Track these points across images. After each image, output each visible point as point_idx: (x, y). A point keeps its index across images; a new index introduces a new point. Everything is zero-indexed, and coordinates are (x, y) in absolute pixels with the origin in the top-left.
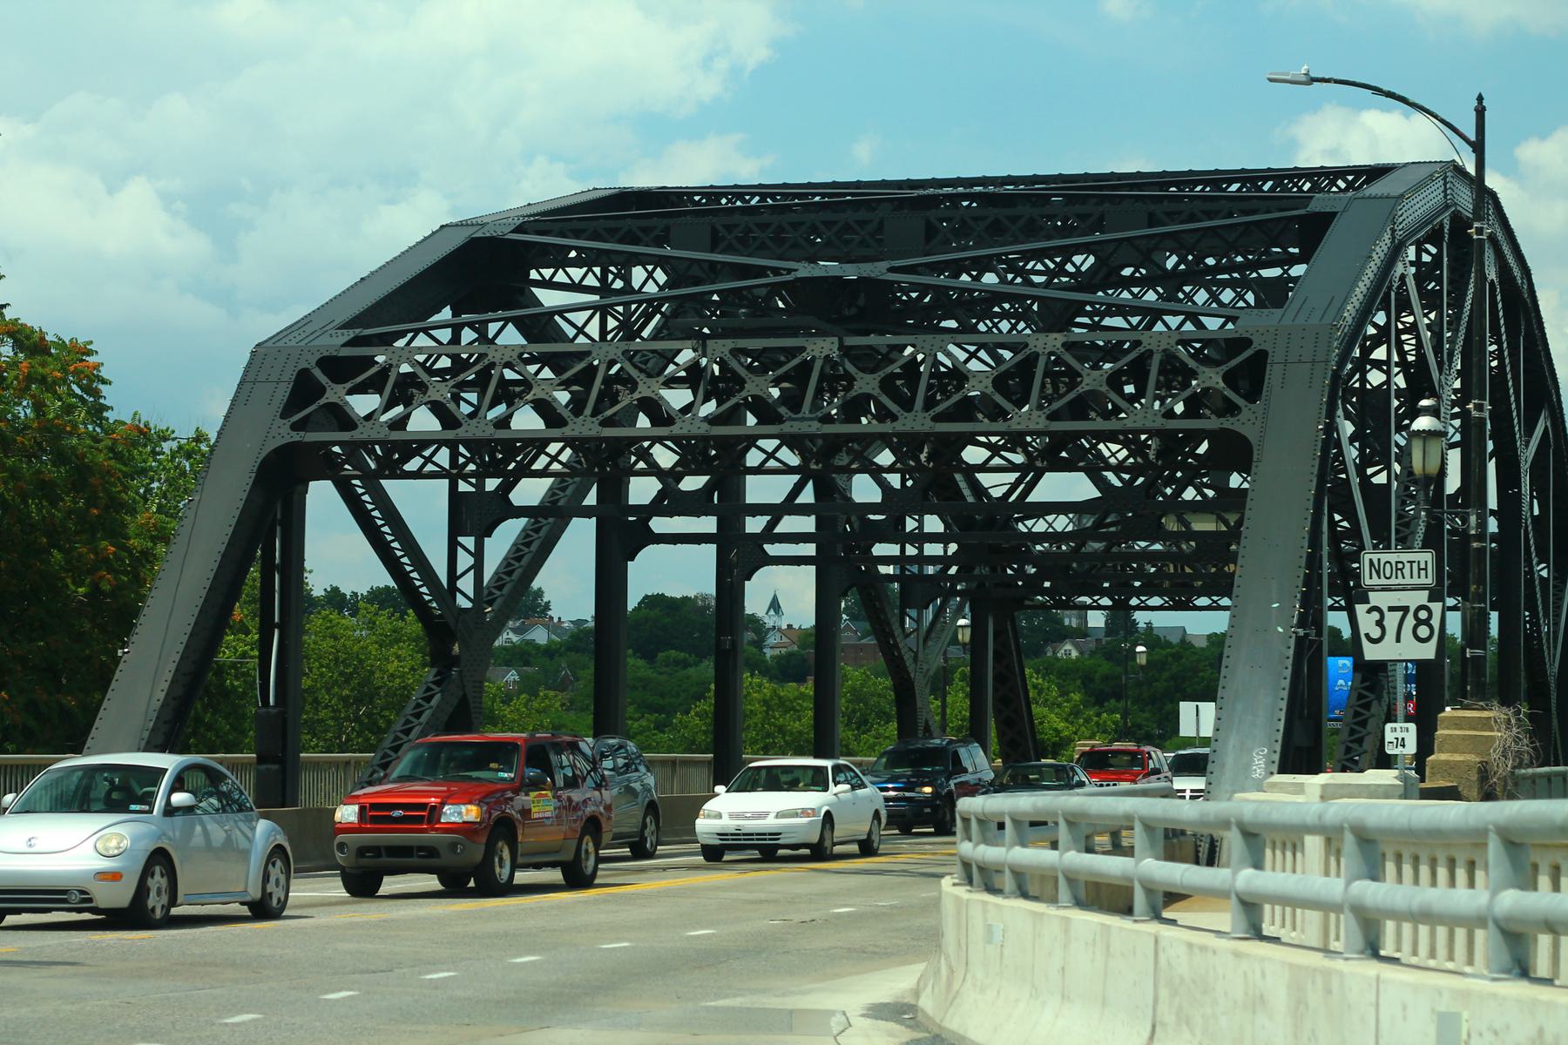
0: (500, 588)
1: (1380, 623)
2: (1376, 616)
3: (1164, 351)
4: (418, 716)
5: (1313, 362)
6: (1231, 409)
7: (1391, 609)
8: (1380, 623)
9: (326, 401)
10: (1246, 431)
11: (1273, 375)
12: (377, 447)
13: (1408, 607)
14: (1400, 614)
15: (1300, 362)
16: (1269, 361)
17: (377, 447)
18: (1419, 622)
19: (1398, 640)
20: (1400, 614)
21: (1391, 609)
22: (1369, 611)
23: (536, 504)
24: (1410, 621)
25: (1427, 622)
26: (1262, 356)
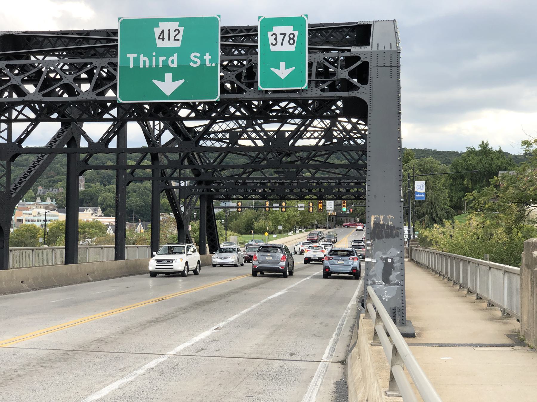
0: (55, 142)
1: (275, 39)
2: (274, 36)
3: (318, 62)
4: (20, 183)
5: (391, 66)
6: (353, 87)
7: (281, 34)
8: (275, 39)
9: (11, 84)
10: (363, 97)
11: (372, 72)
12: (36, 105)
13: (286, 34)
14: (283, 36)
15: (384, 66)
16: (369, 66)
17: (36, 105)
18: (290, 39)
19: (282, 45)
20: (283, 36)
21: (281, 34)
22: (272, 35)
23: (84, 122)
24: (287, 38)
25: (293, 39)
26: (365, 65)
